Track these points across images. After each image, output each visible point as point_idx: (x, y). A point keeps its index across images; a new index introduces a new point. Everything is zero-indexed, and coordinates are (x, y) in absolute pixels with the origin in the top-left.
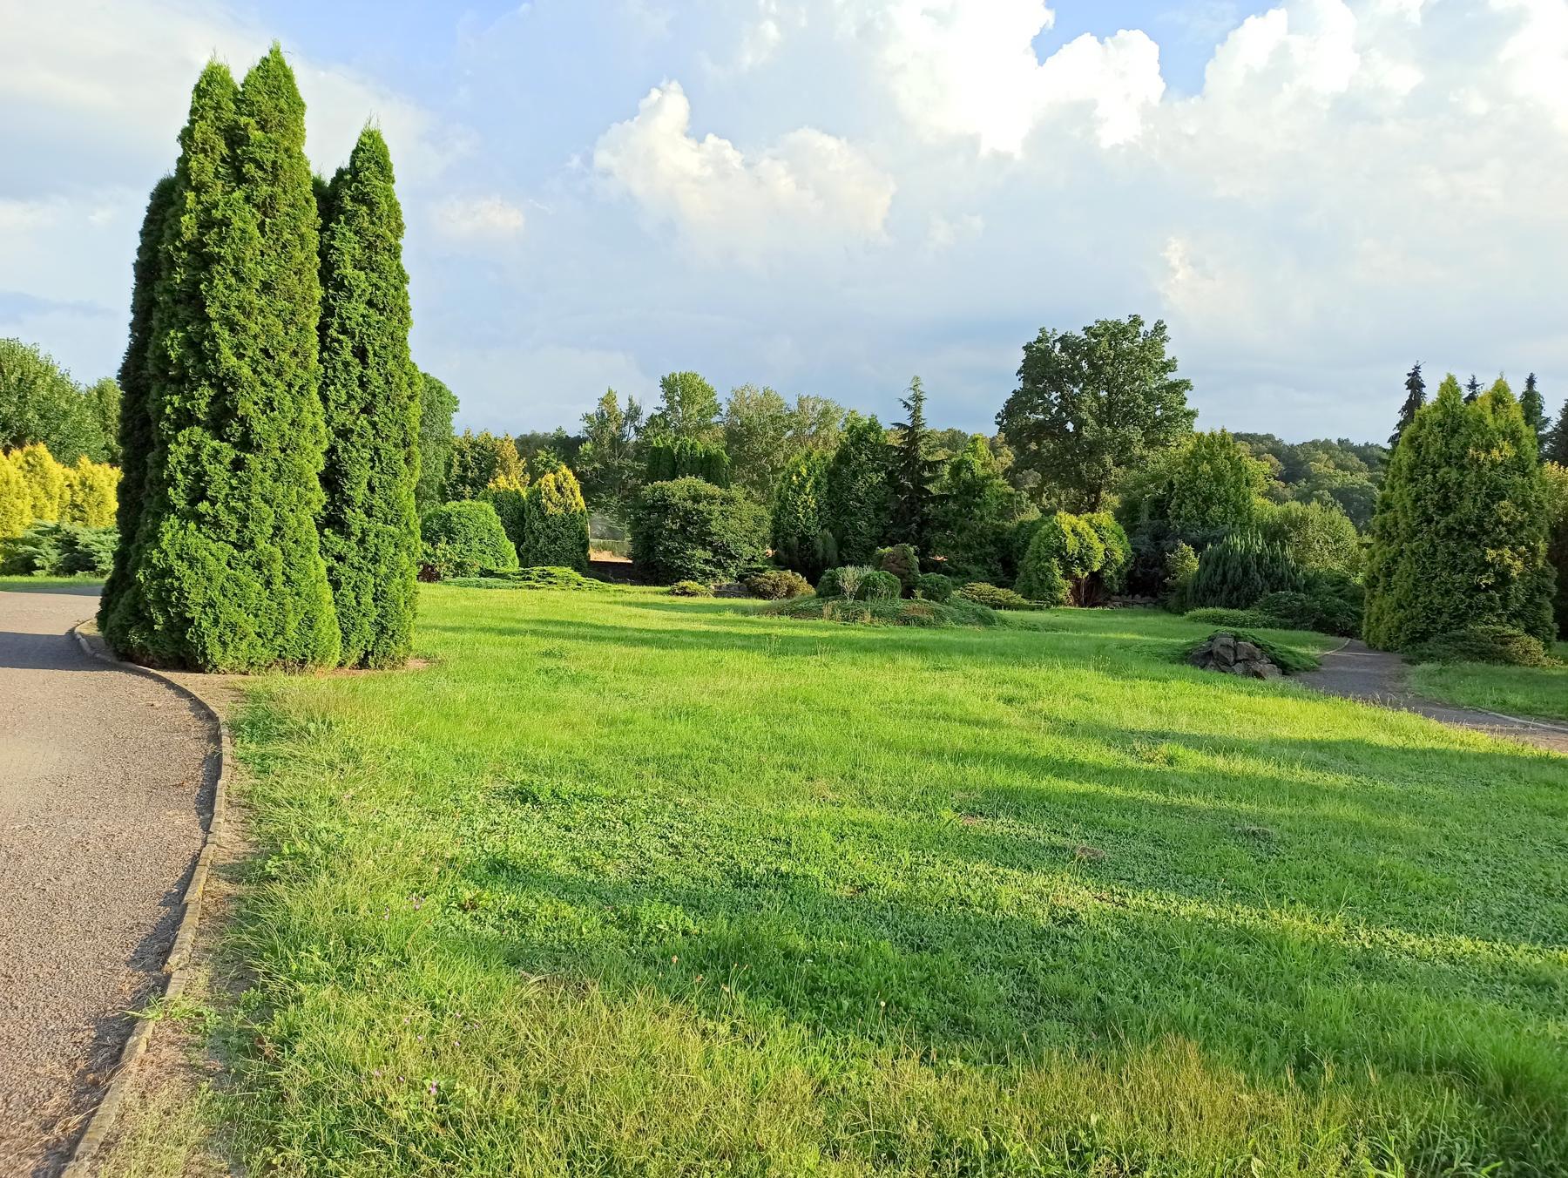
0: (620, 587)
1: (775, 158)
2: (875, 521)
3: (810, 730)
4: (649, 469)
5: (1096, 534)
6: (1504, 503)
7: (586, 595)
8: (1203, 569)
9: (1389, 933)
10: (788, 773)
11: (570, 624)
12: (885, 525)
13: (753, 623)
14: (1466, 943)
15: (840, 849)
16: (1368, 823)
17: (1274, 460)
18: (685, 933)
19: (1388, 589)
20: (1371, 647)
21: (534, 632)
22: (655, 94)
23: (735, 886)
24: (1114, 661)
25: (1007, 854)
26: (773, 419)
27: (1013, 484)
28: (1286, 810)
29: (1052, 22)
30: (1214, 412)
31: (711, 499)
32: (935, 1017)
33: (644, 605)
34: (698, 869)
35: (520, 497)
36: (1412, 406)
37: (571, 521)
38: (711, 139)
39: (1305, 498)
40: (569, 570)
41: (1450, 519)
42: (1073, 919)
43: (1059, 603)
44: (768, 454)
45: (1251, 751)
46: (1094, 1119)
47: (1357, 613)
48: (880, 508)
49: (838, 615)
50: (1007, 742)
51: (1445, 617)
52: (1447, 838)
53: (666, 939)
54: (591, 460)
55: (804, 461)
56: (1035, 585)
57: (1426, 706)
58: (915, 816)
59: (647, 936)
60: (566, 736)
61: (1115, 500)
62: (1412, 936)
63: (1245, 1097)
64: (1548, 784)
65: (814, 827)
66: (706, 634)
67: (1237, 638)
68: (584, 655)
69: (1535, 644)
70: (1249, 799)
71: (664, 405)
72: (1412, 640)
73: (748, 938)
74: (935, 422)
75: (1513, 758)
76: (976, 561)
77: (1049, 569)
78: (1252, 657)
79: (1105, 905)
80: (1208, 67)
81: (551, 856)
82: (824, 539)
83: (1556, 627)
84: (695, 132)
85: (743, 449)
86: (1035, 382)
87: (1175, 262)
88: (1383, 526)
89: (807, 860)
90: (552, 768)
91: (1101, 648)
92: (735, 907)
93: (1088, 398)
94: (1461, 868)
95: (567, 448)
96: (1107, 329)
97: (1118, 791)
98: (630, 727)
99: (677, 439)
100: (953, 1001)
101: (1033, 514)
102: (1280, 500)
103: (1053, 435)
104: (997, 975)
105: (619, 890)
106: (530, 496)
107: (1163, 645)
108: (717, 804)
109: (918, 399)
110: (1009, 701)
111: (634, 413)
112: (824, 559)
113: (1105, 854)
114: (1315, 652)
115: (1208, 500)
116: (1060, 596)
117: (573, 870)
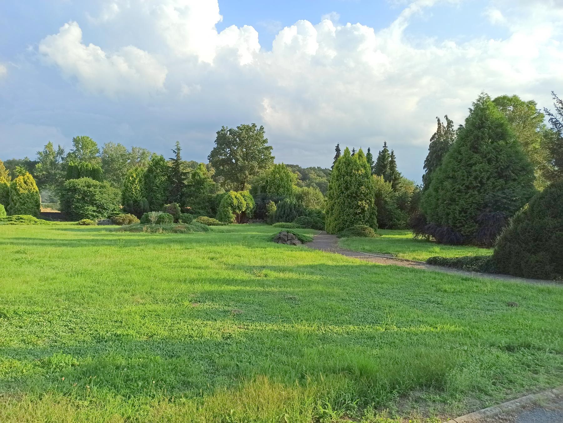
0: (55, 222)
1: (119, 56)
2: (163, 194)
3: (134, 276)
4: (67, 174)
5: (243, 199)
6: (363, 187)
7: (39, 226)
8: (278, 210)
9: (330, 327)
10: (123, 294)
11: (30, 239)
12: (167, 196)
13: (113, 235)
14: (351, 327)
15: (143, 322)
16: (325, 291)
17: (299, 173)
18: (72, 365)
19: (332, 214)
20: (328, 233)
21: (12, 243)
22: (67, 26)
23: (97, 342)
24: (249, 242)
25: (208, 316)
26: (122, 155)
27: (215, 181)
28: (301, 289)
29: (222, 20)
30: (280, 157)
31: (95, 186)
32: (176, 383)
33: (65, 230)
34: (81, 337)
35: (7, 186)
36: (337, 156)
37: (32, 196)
38: (91, 45)
39: (308, 186)
40: (31, 216)
41: (348, 192)
42: (230, 337)
43: (232, 222)
44: (120, 169)
45: (291, 270)
46: (232, 411)
47: (324, 223)
48: (165, 190)
49: (149, 230)
50: (210, 274)
51: (348, 223)
52: (347, 293)
53: (64, 369)
54: (42, 171)
55: (135, 172)
56: (223, 217)
57: (343, 251)
58: (174, 305)
59: (55, 369)
60: (24, 287)
61: (249, 186)
62: (337, 327)
63: (283, 393)
64: (375, 274)
65: (133, 314)
66: (93, 240)
67: (288, 232)
68: (36, 252)
69: (372, 230)
70: (290, 286)
71: (75, 149)
72: (339, 230)
73: (100, 363)
74: (185, 158)
75: (366, 266)
76: (202, 208)
77: (228, 211)
78: (292, 239)
79: (242, 330)
80: (274, 42)
81: (11, 340)
82: (143, 202)
83: (377, 225)
84: (86, 40)
85: (109, 168)
86: (221, 145)
87: (266, 106)
88: (330, 195)
89: (129, 328)
90: (15, 301)
91: (245, 238)
92: (97, 351)
93: (239, 151)
94: (351, 303)
95: (30, 166)
96: (245, 128)
97: (248, 288)
98: (54, 281)
99: (80, 162)
100: (184, 375)
101: (222, 191)
102: (301, 187)
103: (228, 164)
104: (201, 362)
105: (44, 351)
106: (11, 186)
107: (265, 236)
108: (92, 309)
109: (179, 149)
110: (212, 259)
111: (61, 152)
112: (144, 209)
113: (243, 311)
114: (312, 236)
115: (279, 186)
116: (232, 220)
117: (22, 345)
